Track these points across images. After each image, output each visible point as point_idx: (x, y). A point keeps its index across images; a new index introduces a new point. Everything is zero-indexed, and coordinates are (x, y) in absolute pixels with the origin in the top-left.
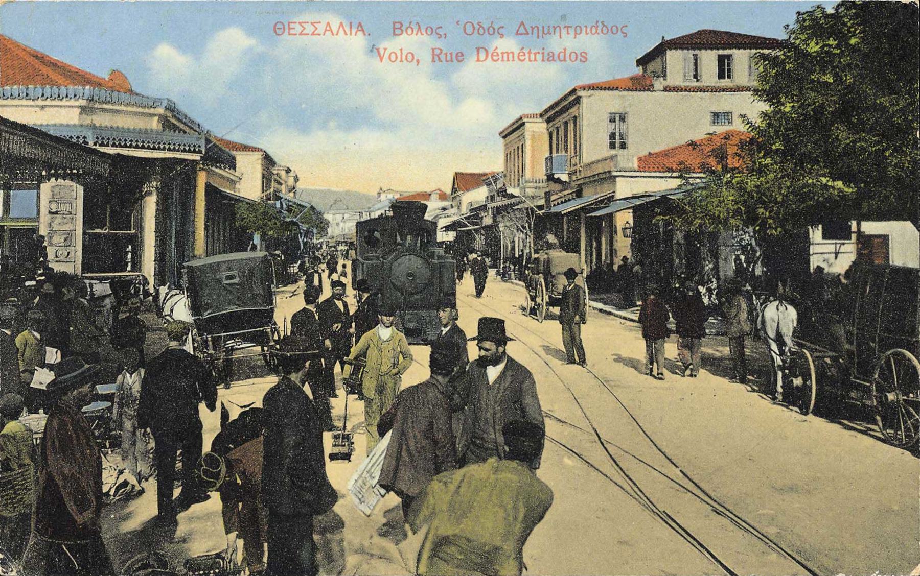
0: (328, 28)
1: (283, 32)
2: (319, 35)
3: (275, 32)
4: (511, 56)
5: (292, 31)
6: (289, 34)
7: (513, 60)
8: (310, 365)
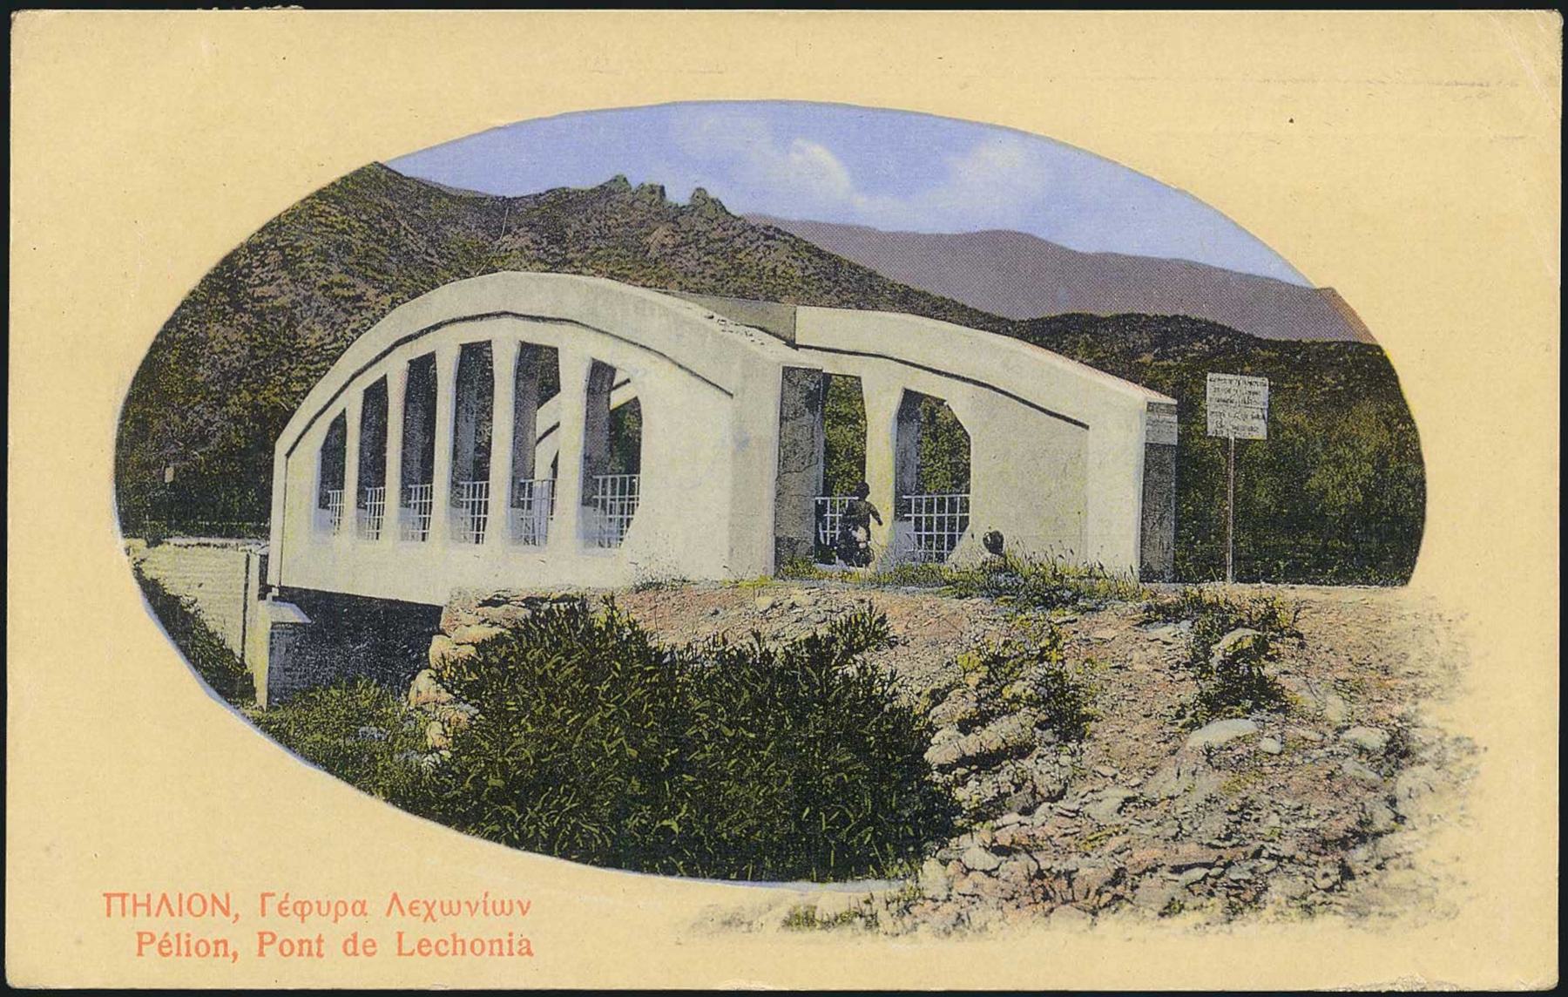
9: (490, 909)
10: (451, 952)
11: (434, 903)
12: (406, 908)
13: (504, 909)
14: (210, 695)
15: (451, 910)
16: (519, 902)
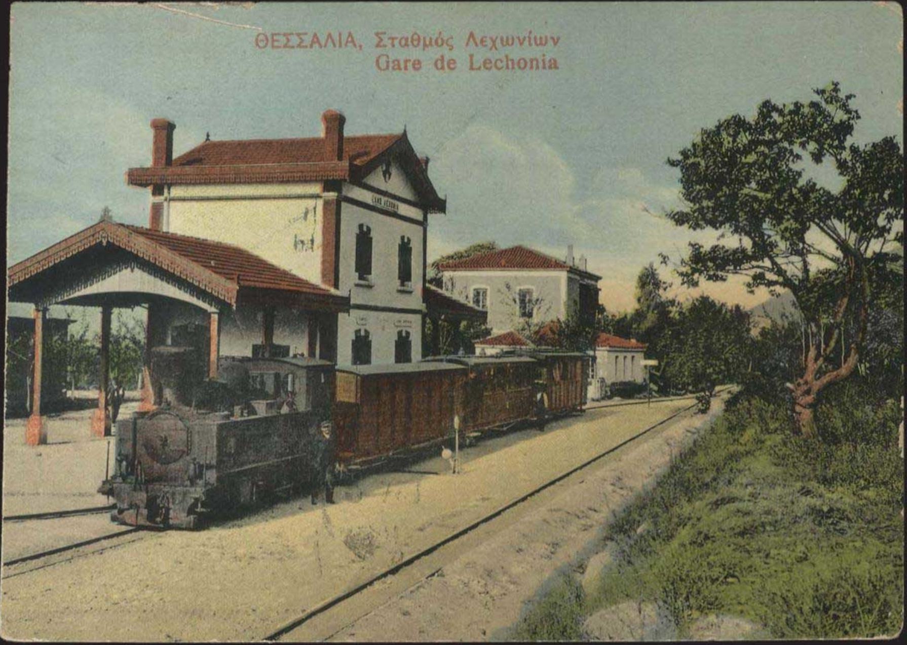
0: (315, 40)
1: (267, 44)
2: (306, 47)
3: (257, 45)
4: (535, 63)
5: (276, 44)
6: (273, 47)
7: (513, 68)
8: (890, 195)
9: (533, 42)
10: (505, 67)
11: (497, 38)
12: (478, 41)
13: (542, 42)
14: (567, 426)
15: (507, 42)
16: (519, 38)
